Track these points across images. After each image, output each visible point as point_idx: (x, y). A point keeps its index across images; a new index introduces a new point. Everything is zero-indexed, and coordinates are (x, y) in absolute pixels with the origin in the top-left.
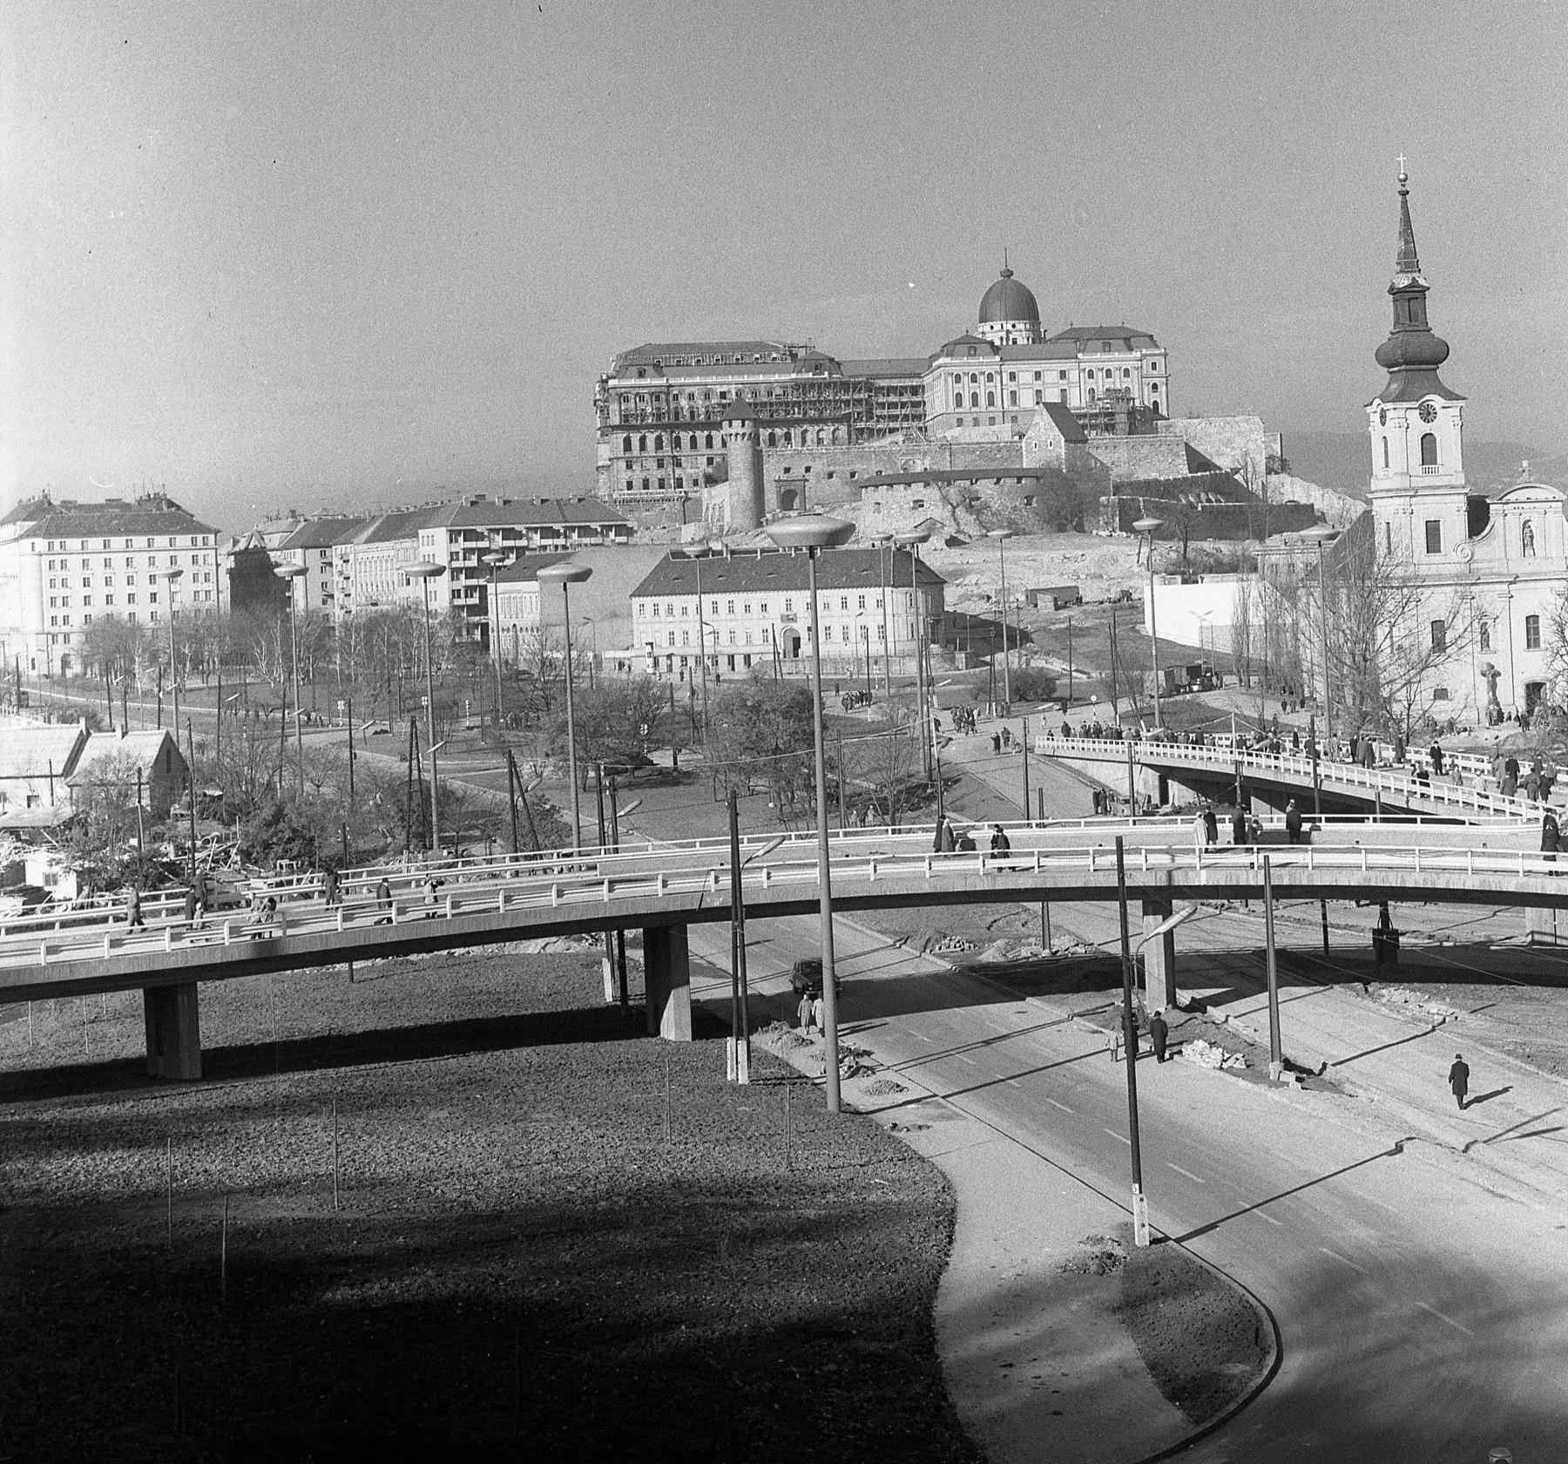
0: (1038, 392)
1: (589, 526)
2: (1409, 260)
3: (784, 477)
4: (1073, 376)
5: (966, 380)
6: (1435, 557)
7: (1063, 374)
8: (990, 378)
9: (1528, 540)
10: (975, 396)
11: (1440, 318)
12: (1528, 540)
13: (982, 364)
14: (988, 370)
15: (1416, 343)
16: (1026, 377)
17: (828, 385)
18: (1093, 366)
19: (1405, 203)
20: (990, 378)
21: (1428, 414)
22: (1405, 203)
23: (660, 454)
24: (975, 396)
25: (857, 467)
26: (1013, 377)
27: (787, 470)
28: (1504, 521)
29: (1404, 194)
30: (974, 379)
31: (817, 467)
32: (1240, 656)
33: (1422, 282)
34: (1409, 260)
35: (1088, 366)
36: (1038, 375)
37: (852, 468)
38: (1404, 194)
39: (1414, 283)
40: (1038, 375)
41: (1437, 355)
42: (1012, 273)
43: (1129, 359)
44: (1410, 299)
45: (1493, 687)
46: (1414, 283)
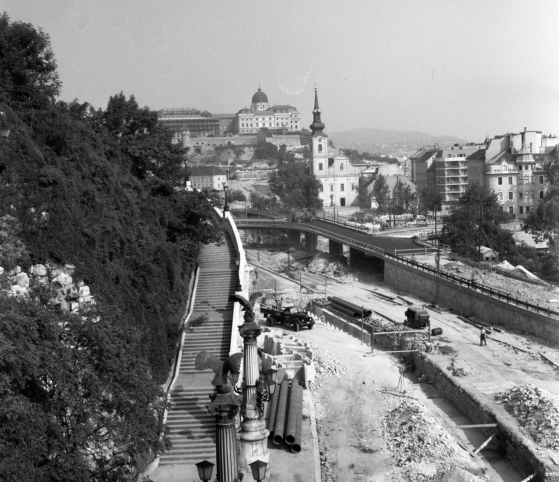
0: (264, 123)
1: (290, 277)
2: (316, 107)
3: (196, 145)
4: (273, 119)
5: (245, 120)
6: (321, 171)
7: (270, 119)
8: (251, 119)
9: (342, 168)
10: (247, 124)
11: (323, 119)
12: (342, 168)
13: (249, 116)
14: (251, 117)
15: (317, 125)
16: (260, 119)
17: (209, 120)
18: (278, 117)
19: (316, 94)
20: (251, 119)
21: (320, 140)
22: (316, 94)
23: (178, 138)
24: (247, 124)
25: (215, 143)
26: (257, 119)
27: (197, 144)
28: (337, 164)
29: (316, 92)
30: (247, 119)
31: (205, 143)
32: (416, 225)
33: (319, 111)
34: (316, 107)
35: (277, 117)
36: (264, 119)
37: (214, 143)
38: (316, 92)
39: (317, 111)
40: (264, 119)
41: (321, 128)
42: (261, 90)
43: (285, 115)
44: (317, 115)
45: (332, 199)
46: (317, 111)
